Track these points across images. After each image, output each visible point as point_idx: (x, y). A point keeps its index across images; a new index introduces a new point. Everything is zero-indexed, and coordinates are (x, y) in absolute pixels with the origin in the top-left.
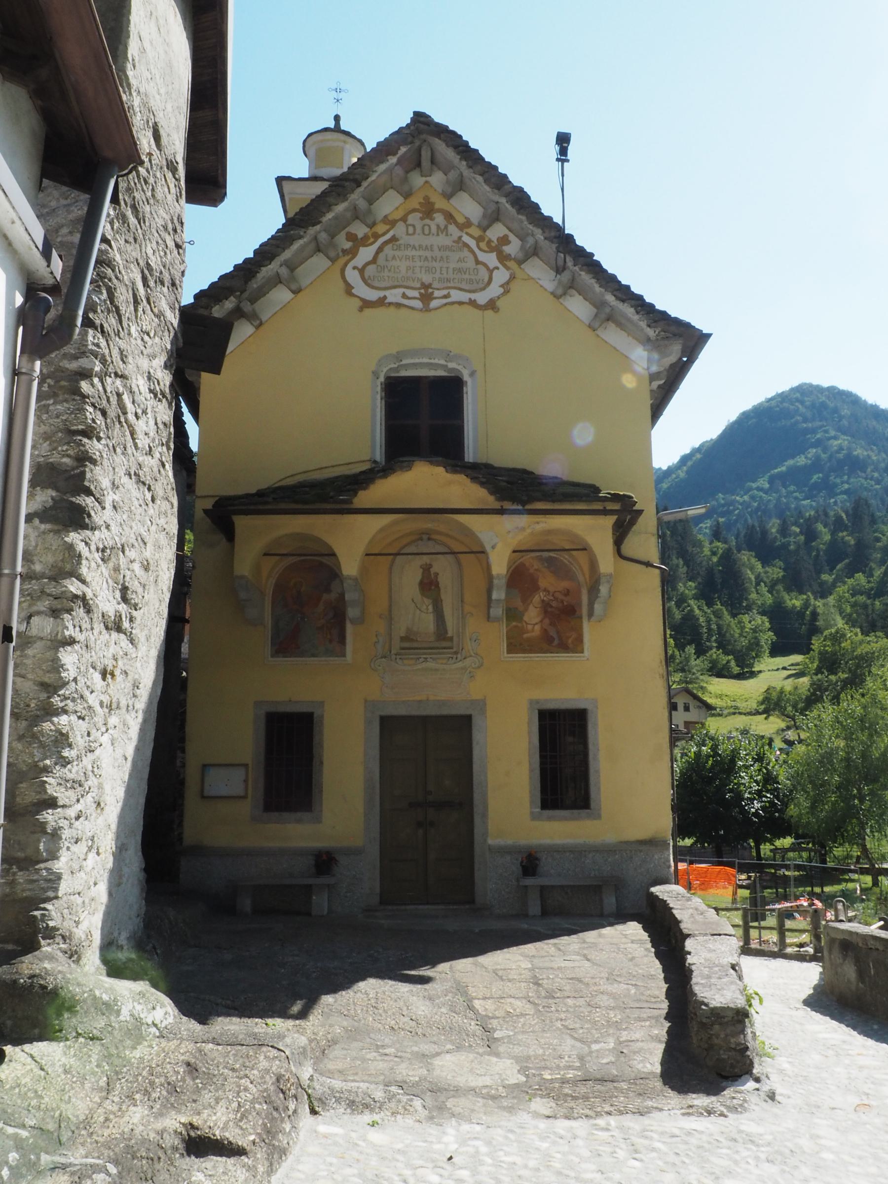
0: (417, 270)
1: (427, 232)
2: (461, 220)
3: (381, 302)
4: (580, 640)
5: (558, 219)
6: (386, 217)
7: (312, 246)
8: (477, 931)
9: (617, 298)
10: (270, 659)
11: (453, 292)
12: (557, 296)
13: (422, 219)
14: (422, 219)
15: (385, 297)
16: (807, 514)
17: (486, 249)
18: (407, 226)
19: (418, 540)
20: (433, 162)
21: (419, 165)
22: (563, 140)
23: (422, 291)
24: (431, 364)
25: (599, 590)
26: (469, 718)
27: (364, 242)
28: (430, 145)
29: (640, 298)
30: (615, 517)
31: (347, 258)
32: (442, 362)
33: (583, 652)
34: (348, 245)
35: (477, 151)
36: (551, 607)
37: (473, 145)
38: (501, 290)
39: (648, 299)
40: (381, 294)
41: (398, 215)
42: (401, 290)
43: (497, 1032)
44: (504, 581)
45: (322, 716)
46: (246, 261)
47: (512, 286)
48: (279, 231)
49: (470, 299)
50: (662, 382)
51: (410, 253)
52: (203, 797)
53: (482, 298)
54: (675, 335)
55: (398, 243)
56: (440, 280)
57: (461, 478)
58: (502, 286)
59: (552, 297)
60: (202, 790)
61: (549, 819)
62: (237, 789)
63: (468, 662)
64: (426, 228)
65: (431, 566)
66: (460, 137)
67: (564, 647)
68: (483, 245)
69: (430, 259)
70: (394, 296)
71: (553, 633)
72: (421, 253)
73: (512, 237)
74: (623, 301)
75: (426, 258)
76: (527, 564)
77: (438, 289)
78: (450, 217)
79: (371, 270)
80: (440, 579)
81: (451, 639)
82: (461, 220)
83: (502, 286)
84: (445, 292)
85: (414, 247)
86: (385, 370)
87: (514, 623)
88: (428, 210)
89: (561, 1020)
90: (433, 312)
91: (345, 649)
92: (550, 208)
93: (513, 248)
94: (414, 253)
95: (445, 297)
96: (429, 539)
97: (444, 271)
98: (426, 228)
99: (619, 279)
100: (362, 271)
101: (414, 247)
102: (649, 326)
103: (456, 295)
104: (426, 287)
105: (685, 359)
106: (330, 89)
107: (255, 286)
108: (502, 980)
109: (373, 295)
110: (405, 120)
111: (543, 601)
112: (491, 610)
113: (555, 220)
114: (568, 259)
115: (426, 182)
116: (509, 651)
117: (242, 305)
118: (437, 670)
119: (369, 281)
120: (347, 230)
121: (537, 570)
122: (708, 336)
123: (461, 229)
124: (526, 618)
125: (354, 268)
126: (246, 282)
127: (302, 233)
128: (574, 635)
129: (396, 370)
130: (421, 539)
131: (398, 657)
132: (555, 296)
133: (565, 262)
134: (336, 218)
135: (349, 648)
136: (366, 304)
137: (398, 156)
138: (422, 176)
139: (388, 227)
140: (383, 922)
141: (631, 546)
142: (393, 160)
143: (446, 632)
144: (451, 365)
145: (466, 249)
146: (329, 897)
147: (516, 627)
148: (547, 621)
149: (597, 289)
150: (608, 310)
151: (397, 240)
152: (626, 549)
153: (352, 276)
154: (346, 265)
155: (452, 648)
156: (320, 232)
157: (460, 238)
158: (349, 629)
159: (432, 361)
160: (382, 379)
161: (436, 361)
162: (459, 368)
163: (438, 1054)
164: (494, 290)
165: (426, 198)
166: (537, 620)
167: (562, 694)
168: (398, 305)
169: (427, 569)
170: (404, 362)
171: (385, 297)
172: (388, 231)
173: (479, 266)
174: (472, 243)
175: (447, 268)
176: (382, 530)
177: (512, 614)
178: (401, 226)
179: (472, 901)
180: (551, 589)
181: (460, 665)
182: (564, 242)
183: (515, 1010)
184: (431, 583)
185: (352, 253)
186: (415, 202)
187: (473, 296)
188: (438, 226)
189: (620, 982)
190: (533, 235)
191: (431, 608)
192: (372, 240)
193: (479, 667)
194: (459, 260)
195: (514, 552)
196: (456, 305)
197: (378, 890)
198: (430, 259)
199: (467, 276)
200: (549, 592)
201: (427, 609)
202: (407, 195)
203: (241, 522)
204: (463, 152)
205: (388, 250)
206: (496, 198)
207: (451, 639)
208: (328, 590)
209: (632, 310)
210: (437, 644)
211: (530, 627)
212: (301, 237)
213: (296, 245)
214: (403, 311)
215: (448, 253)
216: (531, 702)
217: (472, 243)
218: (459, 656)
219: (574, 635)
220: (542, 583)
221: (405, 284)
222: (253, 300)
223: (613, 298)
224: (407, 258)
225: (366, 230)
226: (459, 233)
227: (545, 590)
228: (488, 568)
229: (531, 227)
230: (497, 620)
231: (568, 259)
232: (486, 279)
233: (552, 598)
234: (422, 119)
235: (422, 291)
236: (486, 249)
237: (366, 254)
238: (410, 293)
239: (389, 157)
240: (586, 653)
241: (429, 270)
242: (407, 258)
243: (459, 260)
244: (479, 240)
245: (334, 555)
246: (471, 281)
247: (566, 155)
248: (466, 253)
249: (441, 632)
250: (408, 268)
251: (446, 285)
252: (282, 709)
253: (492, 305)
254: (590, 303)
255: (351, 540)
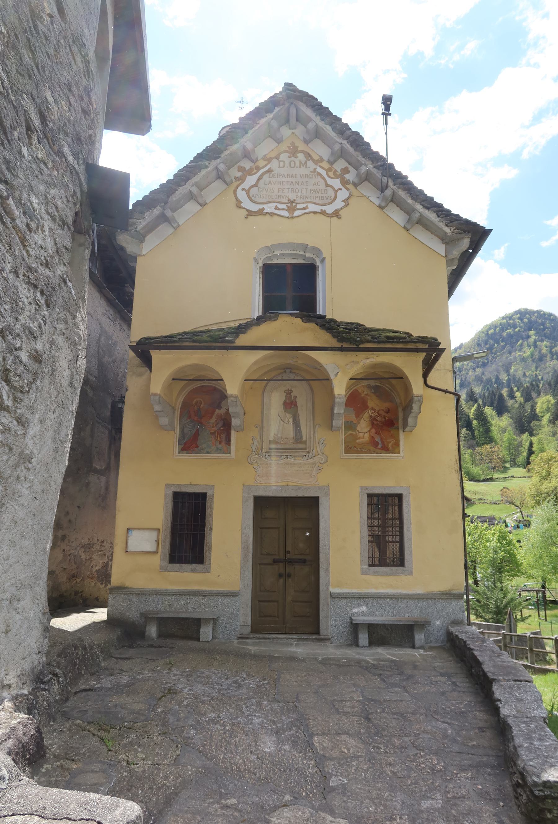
0: (286, 191)
1: (293, 165)
2: (316, 158)
3: (261, 212)
4: (397, 444)
5: (383, 153)
6: (265, 155)
7: (214, 173)
8: (320, 659)
9: (425, 207)
10: (178, 454)
11: (310, 205)
12: (381, 207)
13: (289, 157)
14: (289, 157)
15: (263, 209)
16: (525, 385)
17: (333, 176)
18: (280, 162)
19: (282, 373)
20: (297, 120)
21: (287, 121)
22: (387, 101)
23: (289, 205)
24: (294, 254)
25: (412, 408)
26: (316, 500)
27: (250, 172)
28: (296, 106)
29: (440, 206)
30: (424, 354)
31: (238, 182)
32: (302, 253)
33: (399, 453)
34: (239, 174)
35: (328, 108)
36: (377, 420)
37: (324, 105)
38: (343, 204)
39: (446, 206)
40: (261, 207)
41: (273, 155)
42: (274, 204)
43: (333, 778)
44: (344, 400)
45: (213, 496)
46: (169, 181)
47: (350, 201)
48: (191, 162)
49: (321, 210)
50: (455, 267)
51: (281, 179)
52: (127, 551)
53: (330, 209)
54: (465, 232)
55: (273, 173)
56: (301, 197)
57: (313, 326)
58: (343, 201)
59: (378, 208)
60: (126, 547)
61: (375, 574)
62: (149, 546)
63: (316, 459)
64: (292, 163)
65: (292, 391)
66: (316, 99)
67: (385, 449)
68: (331, 174)
69: (294, 184)
70: (269, 208)
71: (378, 439)
72: (288, 179)
73: (351, 169)
74: (428, 208)
75: (292, 183)
76: (360, 391)
77: (299, 204)
78: (308, 156)
79: (254, 191)
80: (298, 400)
81: (305, 442)
82: (316, 158)
83: (343, 201)
84: (304, 205)
85: (284, 176)
86: (263, 258)
87: (350, 432)
88: (293, 152)
89: (390, 765)
90: (296, 219)
91: (230, 449)
92: (377, 146)
93: (351, 176)
94: (284, 179)
95: (304, 208)
96: (290, 372)
97: (304, 191)
98: (292, 163)
99: (426, 193)
100: (248, 192)
101: (284, 176)
102: (447, 225)
103: (312, 208)
104: (292, 202)
105: (471, 251)
106: (237, 102)
107: (174, 199)
108: (339, 713)
109: (255, 208)
110: (278, 88)
111: (371, 416)
112: (334, 421)
113: (381, 154)
114: (390, 181)
115: (293, 133)
116: (347, 451)
117: (165, 212)
118: (294, 464)
119: (253, 198)
120: (239, 164)
121: (366, 394)
122: (490, 231)
123: (316, 164)
124: (358, 428)
125: (243, 189)
126: (168, 197)
127: (207, 164)
128: (393, 441)
129: (270, 258)
130: (285, 372)
131: (267, 454)
132: (380, 208)
133: (388, 181)
134: (231, 154)
135: (233, 447)
136: (250, 213)
137: (274, 113)
138: (290, 129)
139: (266, 162)
140: (250, 648)
141: (434, 378)
142: (270, 116)
143: (302, 438)
144: (308, 255)
145: (319, 177)
146: (213, 627)
147: (351, 434)
148: (373, 431)
149: (410, 201)
150: (417, 215)
151: (272, 171)
152: (431, 380)
153: (242, 195)
154: (237, 187)
155: (306, 449)
156: (220, 163)
157: (316, 169)
158: (233, 434)
159: (295, 252)
160: (261, 264)
161: (298, 252)
162: (314, 257)
163: (275, 808)
164: (339, 204)
165: (293, 143)
166: (367, 430)
167: (386, 484)
168: (272, 214)
169: (289, 393)
170: (276, 253)
171: (263, 209)
172: (266, 165)
173: (329, 188)
174: (324, 173)
175: (306, 189)
176: (255, 363)
177: (349, 426)
178: (275, 162)
179: (318, 633)
180: (377, 409)
181: (311, 461)
182: (386, 169)
183: (348, 750)
184: (292, 403)
185: (242, 180)
186: (284, 146)
187: (324, 208)
188: (300, 162)
189: (437, 720)
190: (365, 165)
191: (291, 420)
192: (255, 171)
193: (324, 463)
194: (315, 184)
195: (351, 379)
196: (312, 214)
197: (249, 623)
198: (294, 184)
199: (320, 194)
200: (375, 410)
201: (289, 421)
202: (279, 141)
203: (156, 356)
204: (318, 109)
205: (266, 177)
206: (340, 141)
207: (305, 442)
208: (219, 407)
209: (435, 215)
210: (295, 446)
211: (361, 435)
212: (207, 167)
213: (203, 172)
214: (275, 217)
215: (307, 179)
216: (362, 488)
217: (324, 173)
218: (311, 454)
219: (393, 441)
220: (371, 404)
221: (277, 200)
222: (174, 210)
223: (421, 207)
224: (279, 183)
225: (252, 164)
226: (315, 166)
227: (372, 409)
228: (332, 390)
229: (364, 159)
230: (338, 429)
231: (390, 181)
232: (333, 197)
233: (377, 414)
234: (291, 88)
235: (289, 205)
236: (333, 176)
237: (251, 180)
238: (280, 206)
239: (267, 114)
240: (402, 454)
241: (294, 191)
242: (279, 183)
243: (315, 184)
244: (328, 170)
245: (222, 380)
246: (322, 198)
247: (389, 111)
248: (319, 179)
249: (298, 438)
250: (279, 190)
251: (305, 201)
252: (184, 490)
253: (336, 214)
254: (405, 212)
255: (234, 371)
